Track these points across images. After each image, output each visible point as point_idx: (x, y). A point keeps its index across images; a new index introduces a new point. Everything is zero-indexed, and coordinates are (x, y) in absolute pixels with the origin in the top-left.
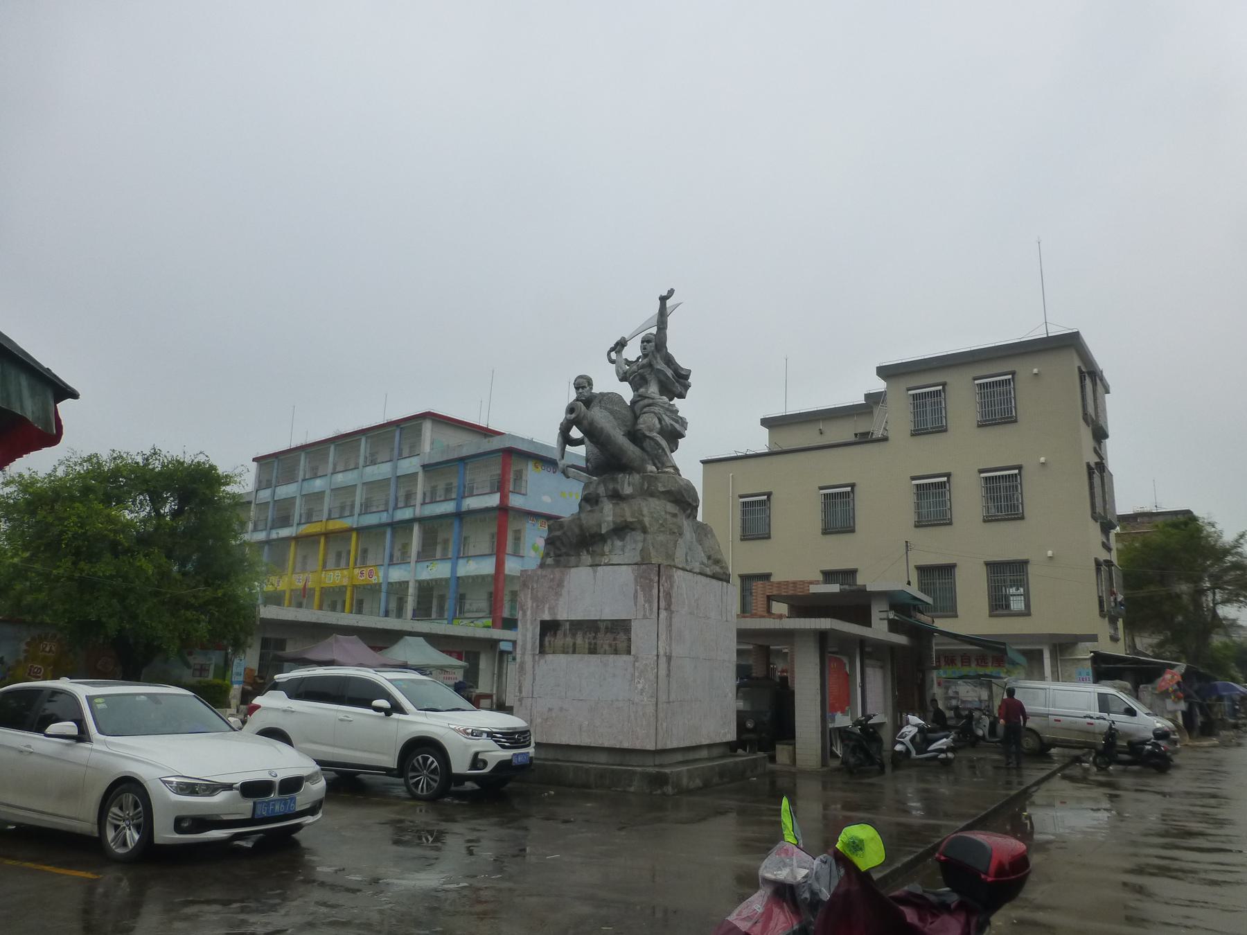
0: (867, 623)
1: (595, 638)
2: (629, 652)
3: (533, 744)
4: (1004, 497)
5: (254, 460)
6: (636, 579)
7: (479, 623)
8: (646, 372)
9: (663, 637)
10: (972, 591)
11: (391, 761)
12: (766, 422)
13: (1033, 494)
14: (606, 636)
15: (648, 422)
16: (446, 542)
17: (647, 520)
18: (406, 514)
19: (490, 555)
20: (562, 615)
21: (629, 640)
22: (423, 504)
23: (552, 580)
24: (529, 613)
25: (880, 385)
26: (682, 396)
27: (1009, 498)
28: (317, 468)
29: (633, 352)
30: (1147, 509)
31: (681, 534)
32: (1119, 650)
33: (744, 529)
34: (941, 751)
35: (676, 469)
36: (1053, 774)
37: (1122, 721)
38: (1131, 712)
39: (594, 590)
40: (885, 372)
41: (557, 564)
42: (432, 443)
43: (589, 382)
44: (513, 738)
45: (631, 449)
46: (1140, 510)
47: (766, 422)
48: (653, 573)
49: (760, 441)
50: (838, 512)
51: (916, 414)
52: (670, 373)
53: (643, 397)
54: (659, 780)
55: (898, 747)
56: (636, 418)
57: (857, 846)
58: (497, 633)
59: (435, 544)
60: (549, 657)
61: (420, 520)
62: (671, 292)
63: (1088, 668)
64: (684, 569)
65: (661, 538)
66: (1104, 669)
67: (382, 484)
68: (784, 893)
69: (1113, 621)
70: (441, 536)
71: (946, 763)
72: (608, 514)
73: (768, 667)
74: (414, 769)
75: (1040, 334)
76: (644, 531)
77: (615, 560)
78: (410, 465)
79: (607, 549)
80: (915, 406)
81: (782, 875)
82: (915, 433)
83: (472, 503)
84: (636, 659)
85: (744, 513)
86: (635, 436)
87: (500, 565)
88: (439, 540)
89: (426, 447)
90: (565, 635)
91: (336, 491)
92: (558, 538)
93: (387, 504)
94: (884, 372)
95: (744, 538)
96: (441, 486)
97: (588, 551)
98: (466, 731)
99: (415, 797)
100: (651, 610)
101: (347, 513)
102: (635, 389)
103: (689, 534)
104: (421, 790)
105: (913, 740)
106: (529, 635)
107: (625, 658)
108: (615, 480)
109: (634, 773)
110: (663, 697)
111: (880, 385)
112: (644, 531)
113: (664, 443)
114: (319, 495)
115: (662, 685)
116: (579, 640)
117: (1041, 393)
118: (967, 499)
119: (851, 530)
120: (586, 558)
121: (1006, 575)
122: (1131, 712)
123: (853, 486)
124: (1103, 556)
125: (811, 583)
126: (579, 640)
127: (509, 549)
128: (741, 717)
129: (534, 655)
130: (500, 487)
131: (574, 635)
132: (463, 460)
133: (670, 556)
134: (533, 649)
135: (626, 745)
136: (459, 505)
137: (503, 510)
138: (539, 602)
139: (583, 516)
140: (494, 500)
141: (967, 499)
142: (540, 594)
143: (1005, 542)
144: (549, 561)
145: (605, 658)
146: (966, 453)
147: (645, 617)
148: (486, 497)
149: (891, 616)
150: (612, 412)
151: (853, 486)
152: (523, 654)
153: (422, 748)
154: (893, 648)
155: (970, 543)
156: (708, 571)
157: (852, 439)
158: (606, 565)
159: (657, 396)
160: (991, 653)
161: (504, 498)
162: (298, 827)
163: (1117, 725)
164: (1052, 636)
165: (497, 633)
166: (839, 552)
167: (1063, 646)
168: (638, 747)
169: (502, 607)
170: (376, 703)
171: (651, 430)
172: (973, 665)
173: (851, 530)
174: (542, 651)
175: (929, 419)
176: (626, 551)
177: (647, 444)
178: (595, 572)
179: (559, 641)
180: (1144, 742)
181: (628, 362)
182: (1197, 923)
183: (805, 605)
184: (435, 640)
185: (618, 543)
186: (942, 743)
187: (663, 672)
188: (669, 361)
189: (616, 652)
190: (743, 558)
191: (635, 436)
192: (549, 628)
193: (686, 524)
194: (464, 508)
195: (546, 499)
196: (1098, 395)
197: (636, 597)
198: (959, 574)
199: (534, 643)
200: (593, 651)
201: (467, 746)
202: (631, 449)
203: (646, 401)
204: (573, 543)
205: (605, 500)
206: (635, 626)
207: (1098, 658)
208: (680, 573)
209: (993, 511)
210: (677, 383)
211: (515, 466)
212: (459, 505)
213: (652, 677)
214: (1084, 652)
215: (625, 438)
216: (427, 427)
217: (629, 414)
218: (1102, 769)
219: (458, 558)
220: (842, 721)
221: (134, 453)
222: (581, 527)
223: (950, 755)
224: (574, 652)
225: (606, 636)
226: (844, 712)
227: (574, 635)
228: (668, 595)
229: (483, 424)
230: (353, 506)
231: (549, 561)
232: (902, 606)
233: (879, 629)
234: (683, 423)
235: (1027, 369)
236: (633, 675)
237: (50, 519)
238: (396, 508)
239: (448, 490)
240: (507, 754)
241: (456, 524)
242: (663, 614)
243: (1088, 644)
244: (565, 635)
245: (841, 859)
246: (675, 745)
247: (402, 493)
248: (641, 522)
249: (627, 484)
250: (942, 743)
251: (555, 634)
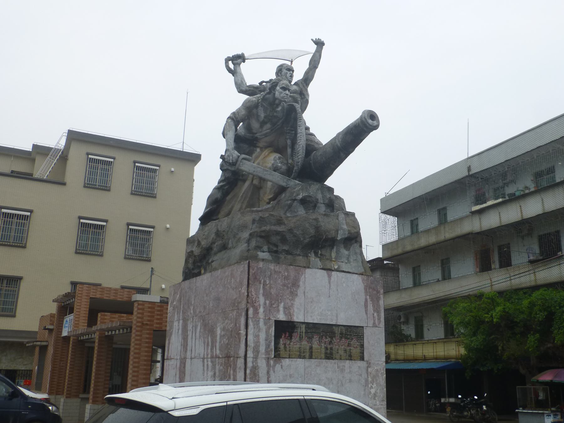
1: (330, 343)
2: (362, 358)
6: (365, 289)
20: (298, 317)
21: (362, 346)
23: (286, 278)
24: (261, 310)
60: (286, 362)
75: (178, 147)
77: (344, 267)
84: (369, 365)
90: (301, 338)
97: (316, 254)
100: (379, 319)
106: (263, 336)
116: (315, 345)
118: (115, 242)
129: (268, 359)
131: (310, 339)
134: (267, 352)
138: (273, 301)
141: (115, 242)
142: (273, 291)
145: (341, 363)
147: (374, 326)
152: (256, 358)
158: (337, 270)
174: (278, 356)
175: (98, 178)
178: (330, 276)
179: (295, 344)
189: (350, 358)
192: (285, 329)
197: (366, 306)
199: (268, 346)
200: (329, 356)
206: (367, 333)
209: (130, 252)
215: (278, 145)
222: (317, 228)
224: (311, 357)
227: (310, 339)
236: (367, 381)
244: (301, 338)
251: (291, 337)
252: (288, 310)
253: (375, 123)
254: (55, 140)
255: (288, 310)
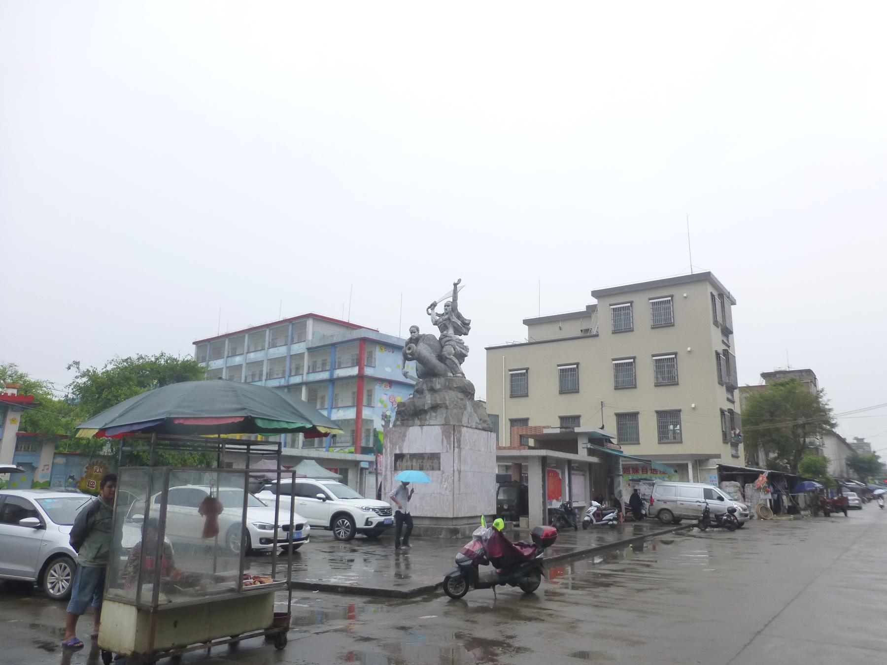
0: (575, 451)
2: (439, 469)
3: (394, 514)
4: (667, 372)
5: (194, 343)
7: (347, 450)
8: (447, 322)
9: (456, 461)
10: (648, 427)
11: (326, 523)
12: (526, 322)
13: (684, 369)
14: (427, 461)
15: (448, 350)
16: (323, 398)
17: (448, 402)
18: (296, 380)
19: (352, 406)
20: (405, 451)
22: (308, 373)
25: (594, 301)
26: (466, 334)
27: (669, 372)
28: (236, 349)
29: (440, 309)
30: (782, 369)
31: (465, 409)
32: (740, 463)
33: (512, 391)
34: (610, 520)
35: (463, 374)
36: (670, 531)
37: (714, 504)
38: (721, 499)
39: (422, 438)
40: (596, 294)
41: (403, 425)
42: (313, 334)
43: (418, 330)
44: (384, 511)
45: (440, 366)
46: (778, 369)
47: (526, 322)
48: (452, 430)
49: (522, 335)
50: (569, 380)
51: (615, 321)
52: (459, 323)
53: (445, 336)
54: (455, 531)
55: (586, 518)
56: (442, 347)
57: (498, 524)
58: (359, 457)
59: (316, 399)
61: (306, 384)
62: (460, 281)
63: (715, 475)
64: (467, 427)
65: (455, 411)
66: (726, 474)
67: (280, 360)
68: (479, 538)
69: (735, 445)
70: (320, 394)
71: (613, 526)
72: (428, 400)
73: (521, 473)
74: (338, 526)
76: (447, 408)
78: (299, 348)
79: (428, 417)
80: (615, 316)
81: (478, 534)
82: (614, 332)
83: (341, 373)
84: (443, 472)
85: (512, 381)
86: (441, 358)
87: (359, 413)
88: (319, 396)
89: (310, 336)
91: (250, 364)
92: (403, 411)
93: (284, 372)
94: (595, 294)
95: (512, 396)
96: (319, 362)
98: (363, 508)
99: (337, 539)
101: (257, 379)
102: (442, 331)
103: (469, 408)
104: (342, 535)
105: (594, 514)
106: (389, 461)
107: (438, 472)
108: (431, 381)
109: (442, 529)
110: (456, 491)
111: (594, 301)
112: (447, 408)
113: (456, 361)
114: (239, 367)
115: (458, 485)
117: (693, 307)
118: (645, 374)
119: (577, 391)
120: (417, 421)
121: (668, 419)
122: (721, 499)
123: (578, 364)
124: (727, 406)
125: (545, 427)
126: (414, 463)
127: (365, 402)
128: (499, 503)
130: (359, 362)
131: (412, 461)
132: (334, 345)
133: (460, 420)
135: (438, 516)
136: (332, 374)
137: (361, 377)
138: (394, 444)
139: (415, 400)
140: (355, 371)
141: (645, 374)
143: (668, 399)
144: (398, 423)
146: (644, 344)
147: (447, 451)
148: (349, 369)
149: (589, 446)
150: (429, 345)
151: (578, 364)
153: (340, 516)
154: (590, 464)
155: (647, 400)
156: (480, 427)
157: (579, 334)
159: (453, 335)
160: (645, 468)
161: (361, 370)
162: (298, 546)
163: (710, 506)
164: (692, 455)
165: (359, 457)
166: (569, 406)
167: (700, 461)
168: (445, 516)
169: (361, 440)
170: (318, 495)
171: (449, 355)
172: (640, 472)
173: (577, 391)
174: (396, 469)
175: (622, 323)
176: (437, 418)
177: (447, 362)
179: (404, 463)
180: (723, 515)
181: (438, 315)
182: (285, 426)
183: (545, 442)
184: (321, 461)
185: (434, 414)
186: (610, 516)
187: (456, 479)
188: (459, 316)
189: (433, 469)
190: (507, 410)
191: (441, 358)
192: (399, 457)
193: (468, 404)
194: (335, 376)
195: (388, 370)
196: (726, 305)
198: (641, 419)
200: (421, 469)
201: (363, 515)
202: (440, 366)
203: (447, 339)
204: (410, 414)
205: (427, 392)
206: (442, 457)
207: (721, 468)
208: (465, 429)
209: (660, 380)
210: (463, 327)
211: (368, 348)
212: (332, 374)
213: (451, 482)
214: (713, 465)
216: (310, 323)
217: (437, 345)
218: (703, 530)
219: (332, 408)
220: (556, 504)
221: (150, 355)
222: (414, 406)
223: (615, 522)
225: (427, 461)
226: (557, 500)
227: (412, 461)
228: (459, 441)
229: (346, 320)
230: (261, 375)
231: (398, 423)
232: (597, 441)
233: (582, 455)
234: (467, 349)
235: (681, 293)
237: (109, 397)
238: (290, 376)
239: (324, 364)
240: (382, 519)
241: (330, 386)
242: (456, 450)
243: (715, 460)
245: (494, 528)
246: (463, 515)
247: (294, 366)
248: (445, 404)
249: (438, 383)
250: (610, 516)
252: (400, 448)
253: (464, 330)
254: (581, 302)
255: (400, 448)
